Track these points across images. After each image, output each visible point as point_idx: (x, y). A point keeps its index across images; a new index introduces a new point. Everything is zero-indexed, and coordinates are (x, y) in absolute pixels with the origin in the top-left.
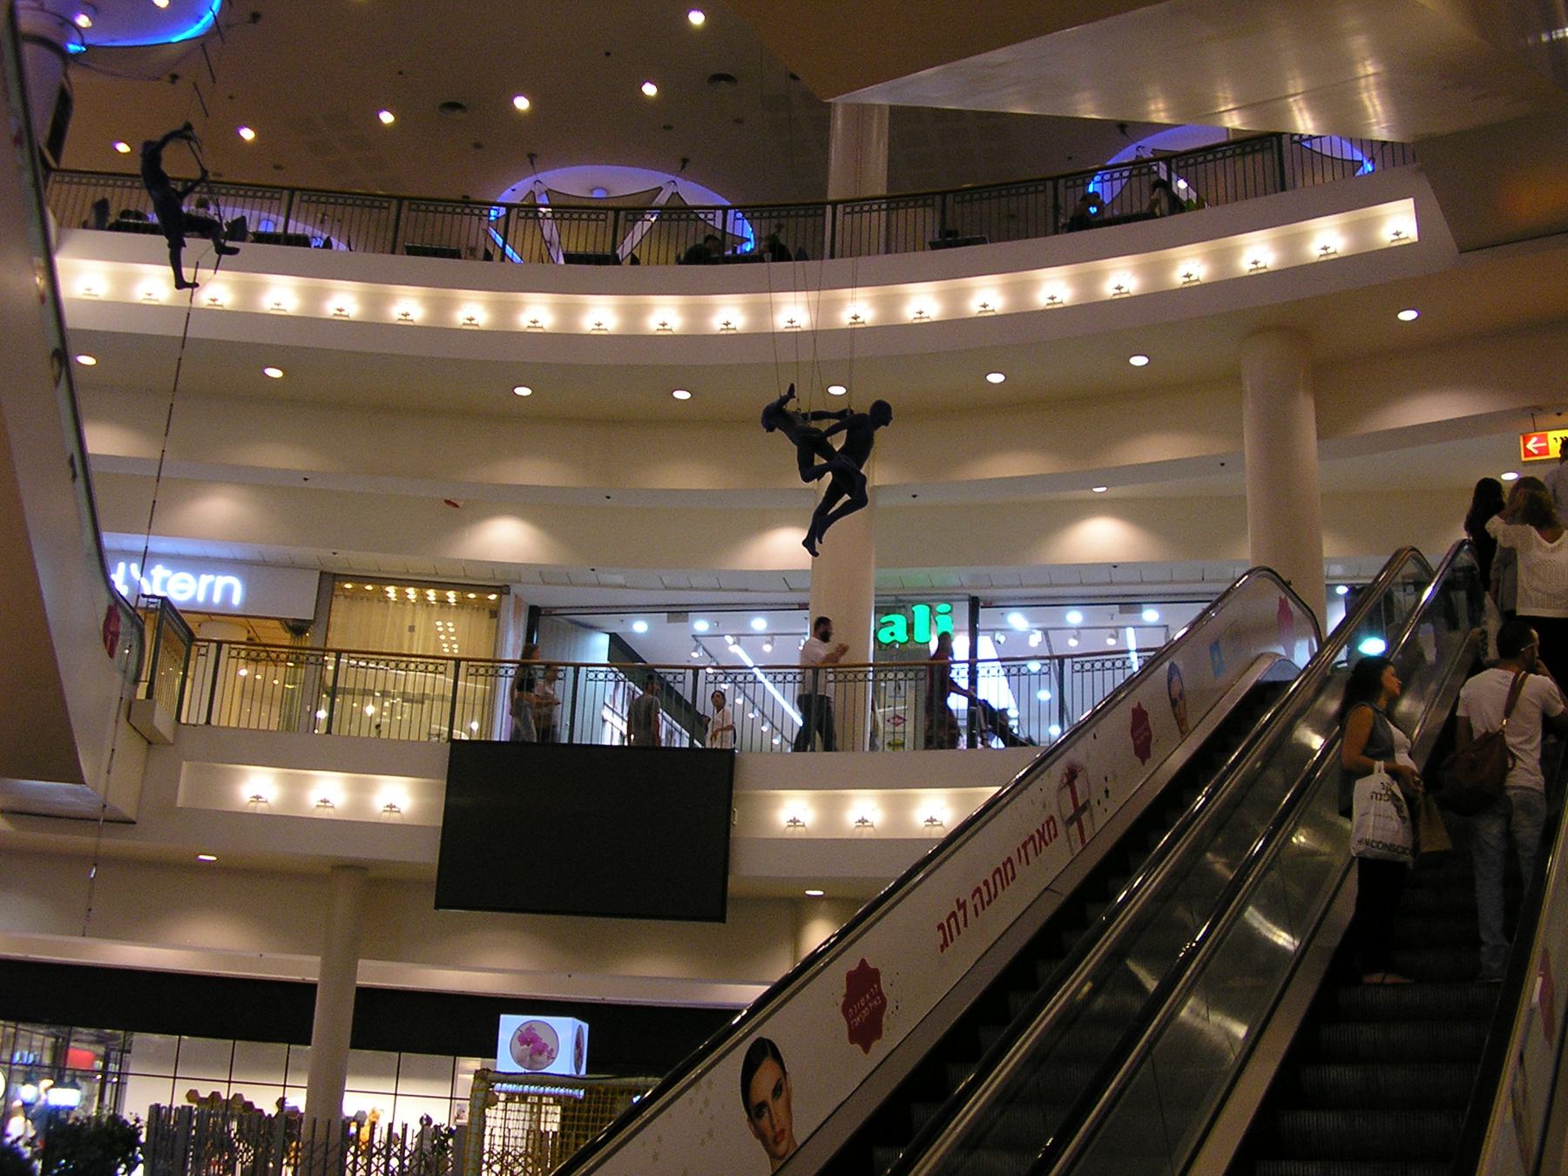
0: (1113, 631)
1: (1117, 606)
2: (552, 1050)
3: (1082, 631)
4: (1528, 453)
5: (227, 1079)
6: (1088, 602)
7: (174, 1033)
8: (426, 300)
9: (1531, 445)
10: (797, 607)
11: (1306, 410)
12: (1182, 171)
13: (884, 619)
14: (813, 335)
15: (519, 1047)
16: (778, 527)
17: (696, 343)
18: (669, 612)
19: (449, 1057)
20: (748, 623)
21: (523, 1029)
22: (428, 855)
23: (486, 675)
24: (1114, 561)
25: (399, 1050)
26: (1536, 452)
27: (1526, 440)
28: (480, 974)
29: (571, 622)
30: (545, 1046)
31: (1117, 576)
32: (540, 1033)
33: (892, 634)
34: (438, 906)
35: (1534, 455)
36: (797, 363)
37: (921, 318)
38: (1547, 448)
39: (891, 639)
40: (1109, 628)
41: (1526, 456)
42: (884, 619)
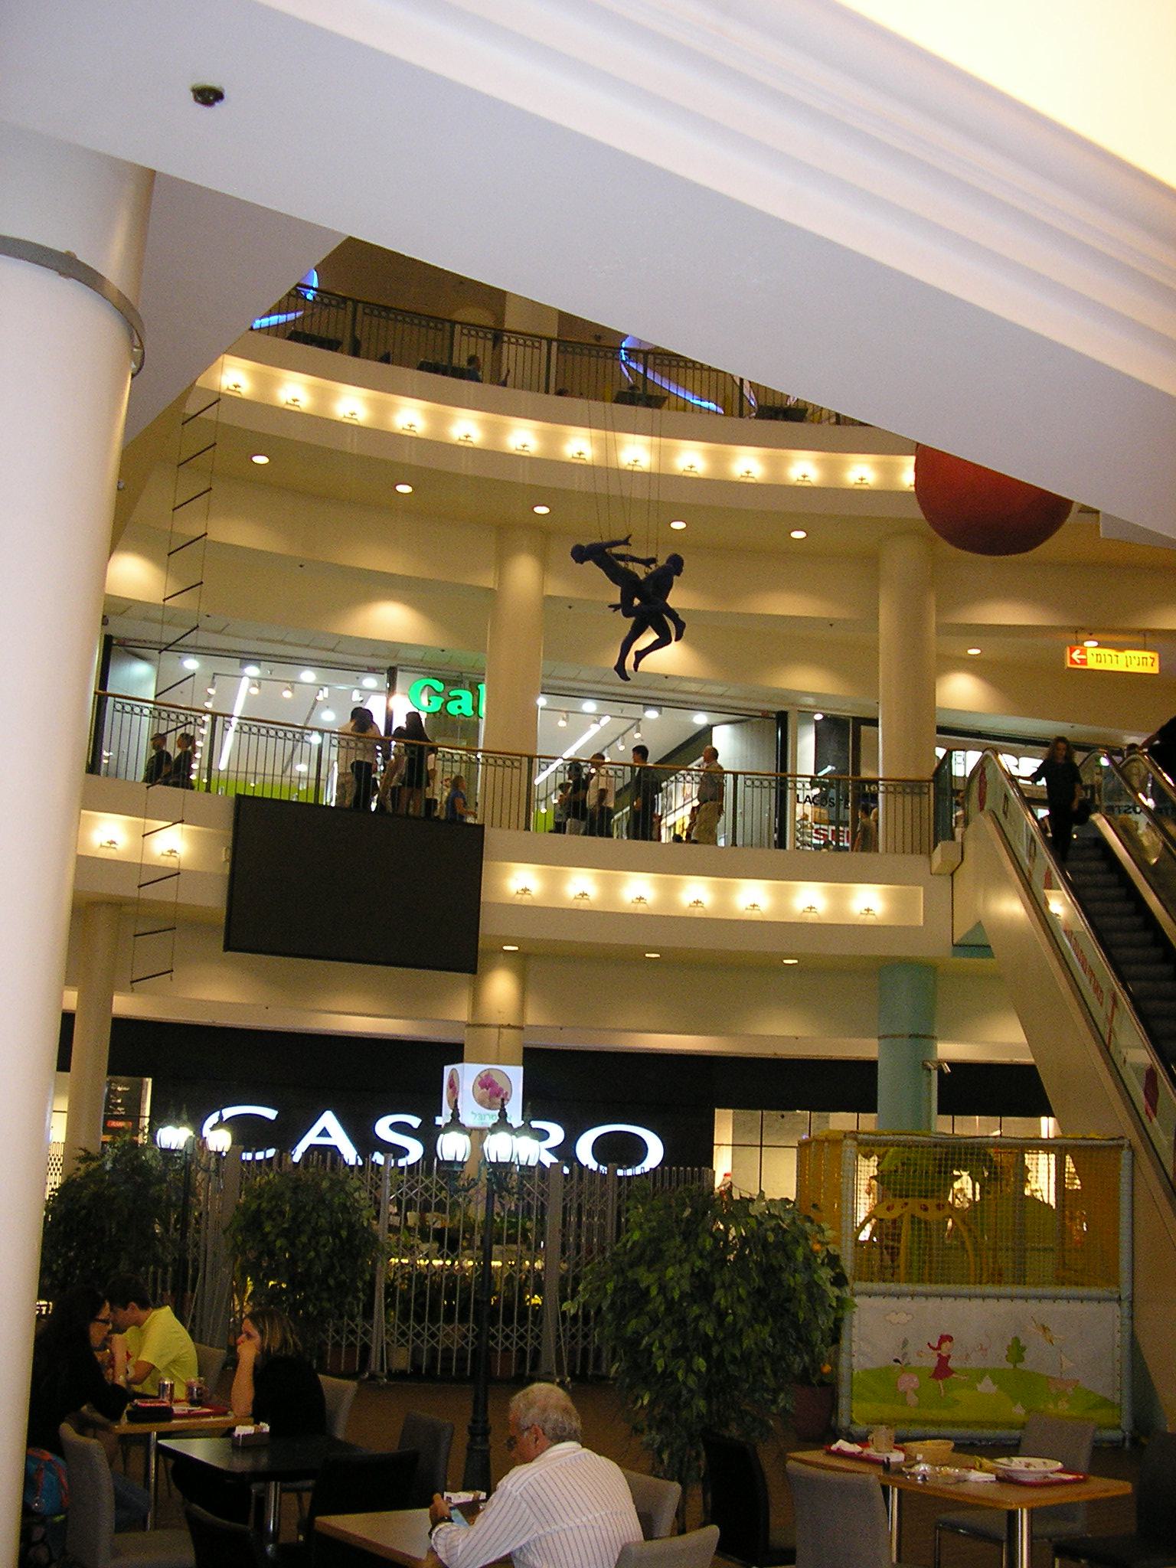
0: (288, 685)
1: (238, 660)
2: (507, 1093)
3: (263, 681)
4: (1073, 661)
5: (759, 1148)
6: (608, 698)
7: (756, 1108)
8: (820, 463)
9: (1076, 655)
10: (366, 669)
11: (932, 600)
12: (318, 299)
13: (453, 693)
14: (648, 477)
15: (480, 1091)
16: (389, 599)
17: (549, 465)
18: (644, 704)
19: (850, 1114)
20: (298, 674)
21: (483, 1075)
22: (213, 898)
23: (912, 793)
24: (667, 673)
25: (1001, 1114)
26: (1078, 661)
27: (1072, 651)
28: (669, 1036)
29: (126, 650)
30: (501, 1090)
31: (668, 684)
32: (496, 1078)
33: (460, 707)
34: (227, 948)
35: (1076, 663)
36: (622, 497)
37: (466, 441)
38: (1086, 660)
39: (459, 711)
40: (287, 682)
41: (1071, 663)
42: (453, 693)
